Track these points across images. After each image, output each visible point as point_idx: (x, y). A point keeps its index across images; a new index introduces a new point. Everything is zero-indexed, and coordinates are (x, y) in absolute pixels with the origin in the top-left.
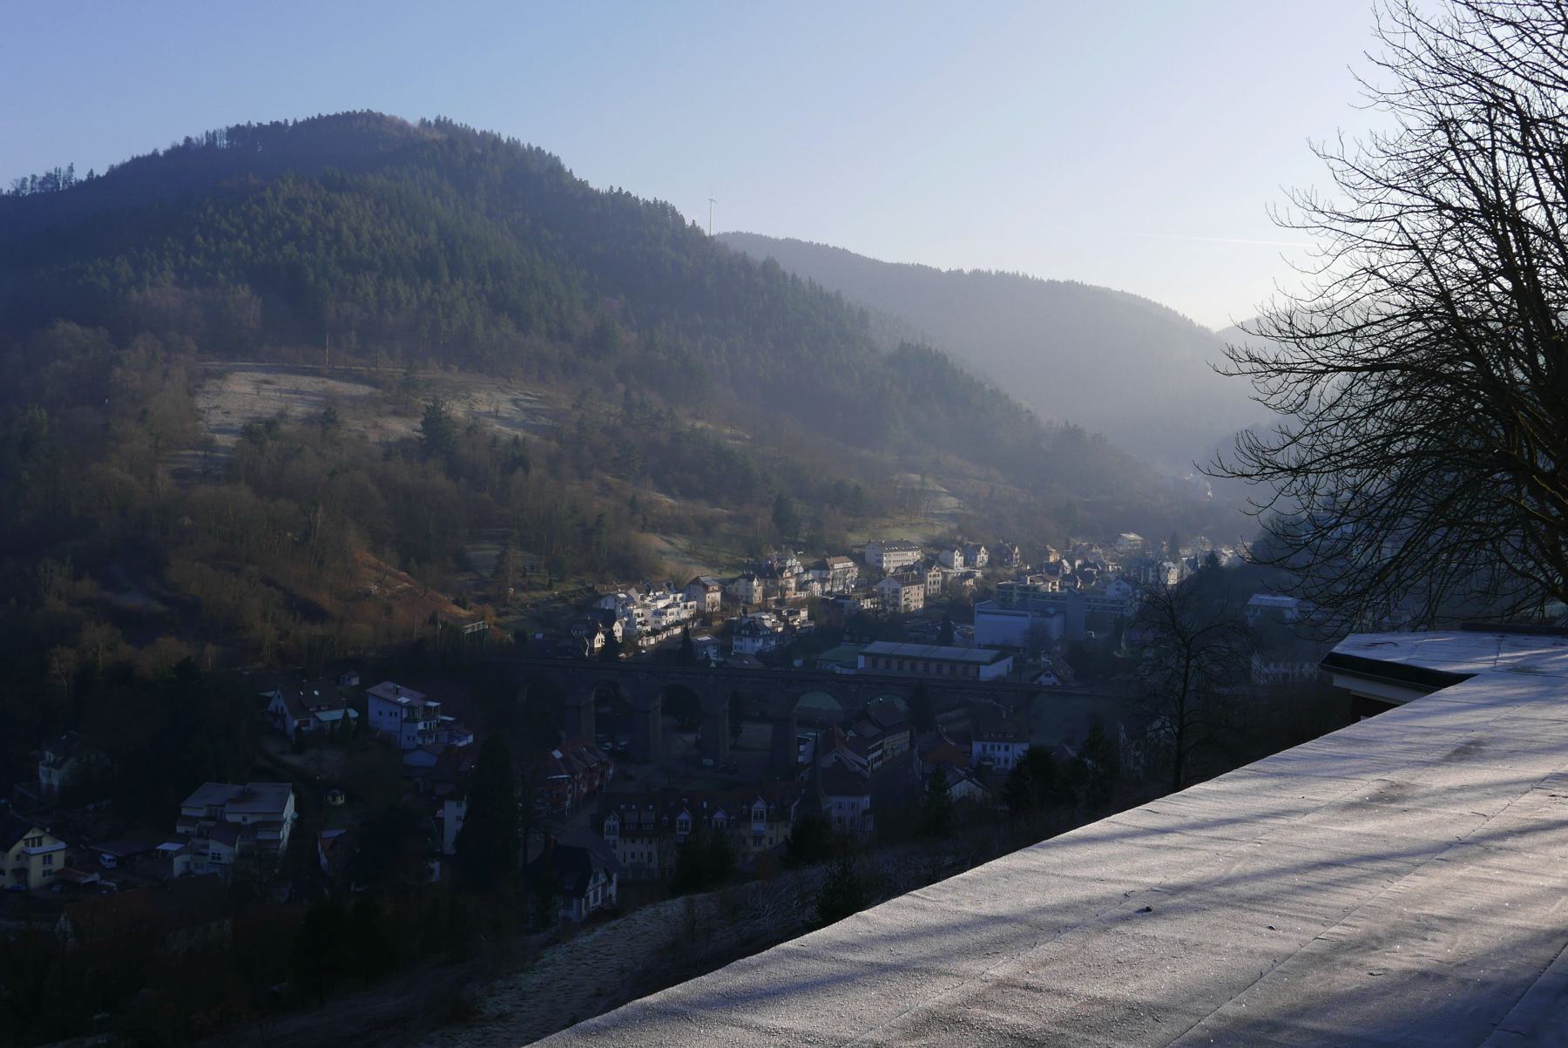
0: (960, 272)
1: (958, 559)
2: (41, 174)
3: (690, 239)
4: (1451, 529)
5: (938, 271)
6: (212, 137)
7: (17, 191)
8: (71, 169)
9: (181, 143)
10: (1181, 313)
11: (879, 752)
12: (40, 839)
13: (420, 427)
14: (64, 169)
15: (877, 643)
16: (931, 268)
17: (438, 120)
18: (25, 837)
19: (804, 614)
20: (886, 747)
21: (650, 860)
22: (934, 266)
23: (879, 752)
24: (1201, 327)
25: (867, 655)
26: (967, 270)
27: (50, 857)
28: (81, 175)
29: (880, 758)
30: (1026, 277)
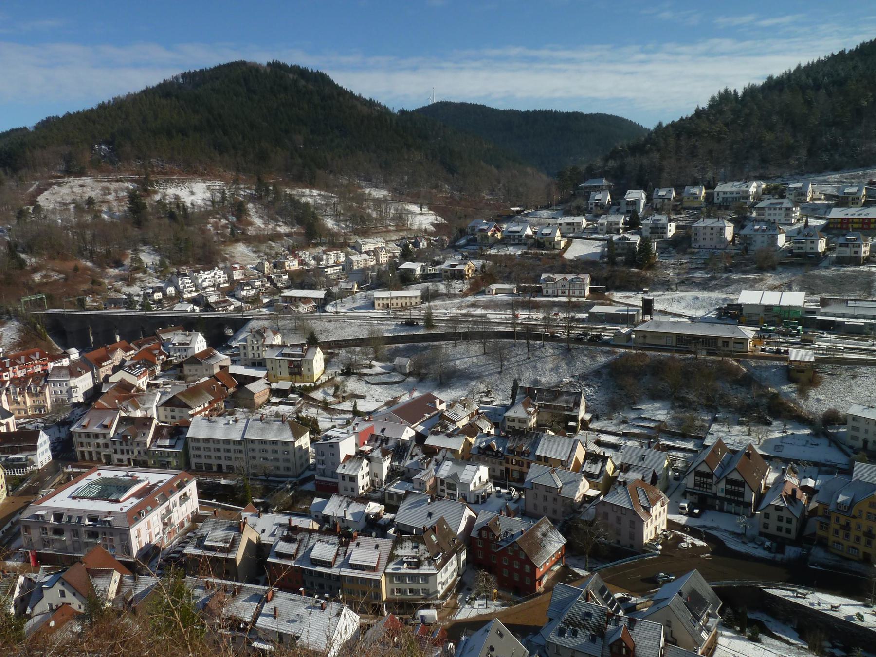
0: (528, 111)
6: (177, 78)
9: (162, 82)
17: (273, 62)
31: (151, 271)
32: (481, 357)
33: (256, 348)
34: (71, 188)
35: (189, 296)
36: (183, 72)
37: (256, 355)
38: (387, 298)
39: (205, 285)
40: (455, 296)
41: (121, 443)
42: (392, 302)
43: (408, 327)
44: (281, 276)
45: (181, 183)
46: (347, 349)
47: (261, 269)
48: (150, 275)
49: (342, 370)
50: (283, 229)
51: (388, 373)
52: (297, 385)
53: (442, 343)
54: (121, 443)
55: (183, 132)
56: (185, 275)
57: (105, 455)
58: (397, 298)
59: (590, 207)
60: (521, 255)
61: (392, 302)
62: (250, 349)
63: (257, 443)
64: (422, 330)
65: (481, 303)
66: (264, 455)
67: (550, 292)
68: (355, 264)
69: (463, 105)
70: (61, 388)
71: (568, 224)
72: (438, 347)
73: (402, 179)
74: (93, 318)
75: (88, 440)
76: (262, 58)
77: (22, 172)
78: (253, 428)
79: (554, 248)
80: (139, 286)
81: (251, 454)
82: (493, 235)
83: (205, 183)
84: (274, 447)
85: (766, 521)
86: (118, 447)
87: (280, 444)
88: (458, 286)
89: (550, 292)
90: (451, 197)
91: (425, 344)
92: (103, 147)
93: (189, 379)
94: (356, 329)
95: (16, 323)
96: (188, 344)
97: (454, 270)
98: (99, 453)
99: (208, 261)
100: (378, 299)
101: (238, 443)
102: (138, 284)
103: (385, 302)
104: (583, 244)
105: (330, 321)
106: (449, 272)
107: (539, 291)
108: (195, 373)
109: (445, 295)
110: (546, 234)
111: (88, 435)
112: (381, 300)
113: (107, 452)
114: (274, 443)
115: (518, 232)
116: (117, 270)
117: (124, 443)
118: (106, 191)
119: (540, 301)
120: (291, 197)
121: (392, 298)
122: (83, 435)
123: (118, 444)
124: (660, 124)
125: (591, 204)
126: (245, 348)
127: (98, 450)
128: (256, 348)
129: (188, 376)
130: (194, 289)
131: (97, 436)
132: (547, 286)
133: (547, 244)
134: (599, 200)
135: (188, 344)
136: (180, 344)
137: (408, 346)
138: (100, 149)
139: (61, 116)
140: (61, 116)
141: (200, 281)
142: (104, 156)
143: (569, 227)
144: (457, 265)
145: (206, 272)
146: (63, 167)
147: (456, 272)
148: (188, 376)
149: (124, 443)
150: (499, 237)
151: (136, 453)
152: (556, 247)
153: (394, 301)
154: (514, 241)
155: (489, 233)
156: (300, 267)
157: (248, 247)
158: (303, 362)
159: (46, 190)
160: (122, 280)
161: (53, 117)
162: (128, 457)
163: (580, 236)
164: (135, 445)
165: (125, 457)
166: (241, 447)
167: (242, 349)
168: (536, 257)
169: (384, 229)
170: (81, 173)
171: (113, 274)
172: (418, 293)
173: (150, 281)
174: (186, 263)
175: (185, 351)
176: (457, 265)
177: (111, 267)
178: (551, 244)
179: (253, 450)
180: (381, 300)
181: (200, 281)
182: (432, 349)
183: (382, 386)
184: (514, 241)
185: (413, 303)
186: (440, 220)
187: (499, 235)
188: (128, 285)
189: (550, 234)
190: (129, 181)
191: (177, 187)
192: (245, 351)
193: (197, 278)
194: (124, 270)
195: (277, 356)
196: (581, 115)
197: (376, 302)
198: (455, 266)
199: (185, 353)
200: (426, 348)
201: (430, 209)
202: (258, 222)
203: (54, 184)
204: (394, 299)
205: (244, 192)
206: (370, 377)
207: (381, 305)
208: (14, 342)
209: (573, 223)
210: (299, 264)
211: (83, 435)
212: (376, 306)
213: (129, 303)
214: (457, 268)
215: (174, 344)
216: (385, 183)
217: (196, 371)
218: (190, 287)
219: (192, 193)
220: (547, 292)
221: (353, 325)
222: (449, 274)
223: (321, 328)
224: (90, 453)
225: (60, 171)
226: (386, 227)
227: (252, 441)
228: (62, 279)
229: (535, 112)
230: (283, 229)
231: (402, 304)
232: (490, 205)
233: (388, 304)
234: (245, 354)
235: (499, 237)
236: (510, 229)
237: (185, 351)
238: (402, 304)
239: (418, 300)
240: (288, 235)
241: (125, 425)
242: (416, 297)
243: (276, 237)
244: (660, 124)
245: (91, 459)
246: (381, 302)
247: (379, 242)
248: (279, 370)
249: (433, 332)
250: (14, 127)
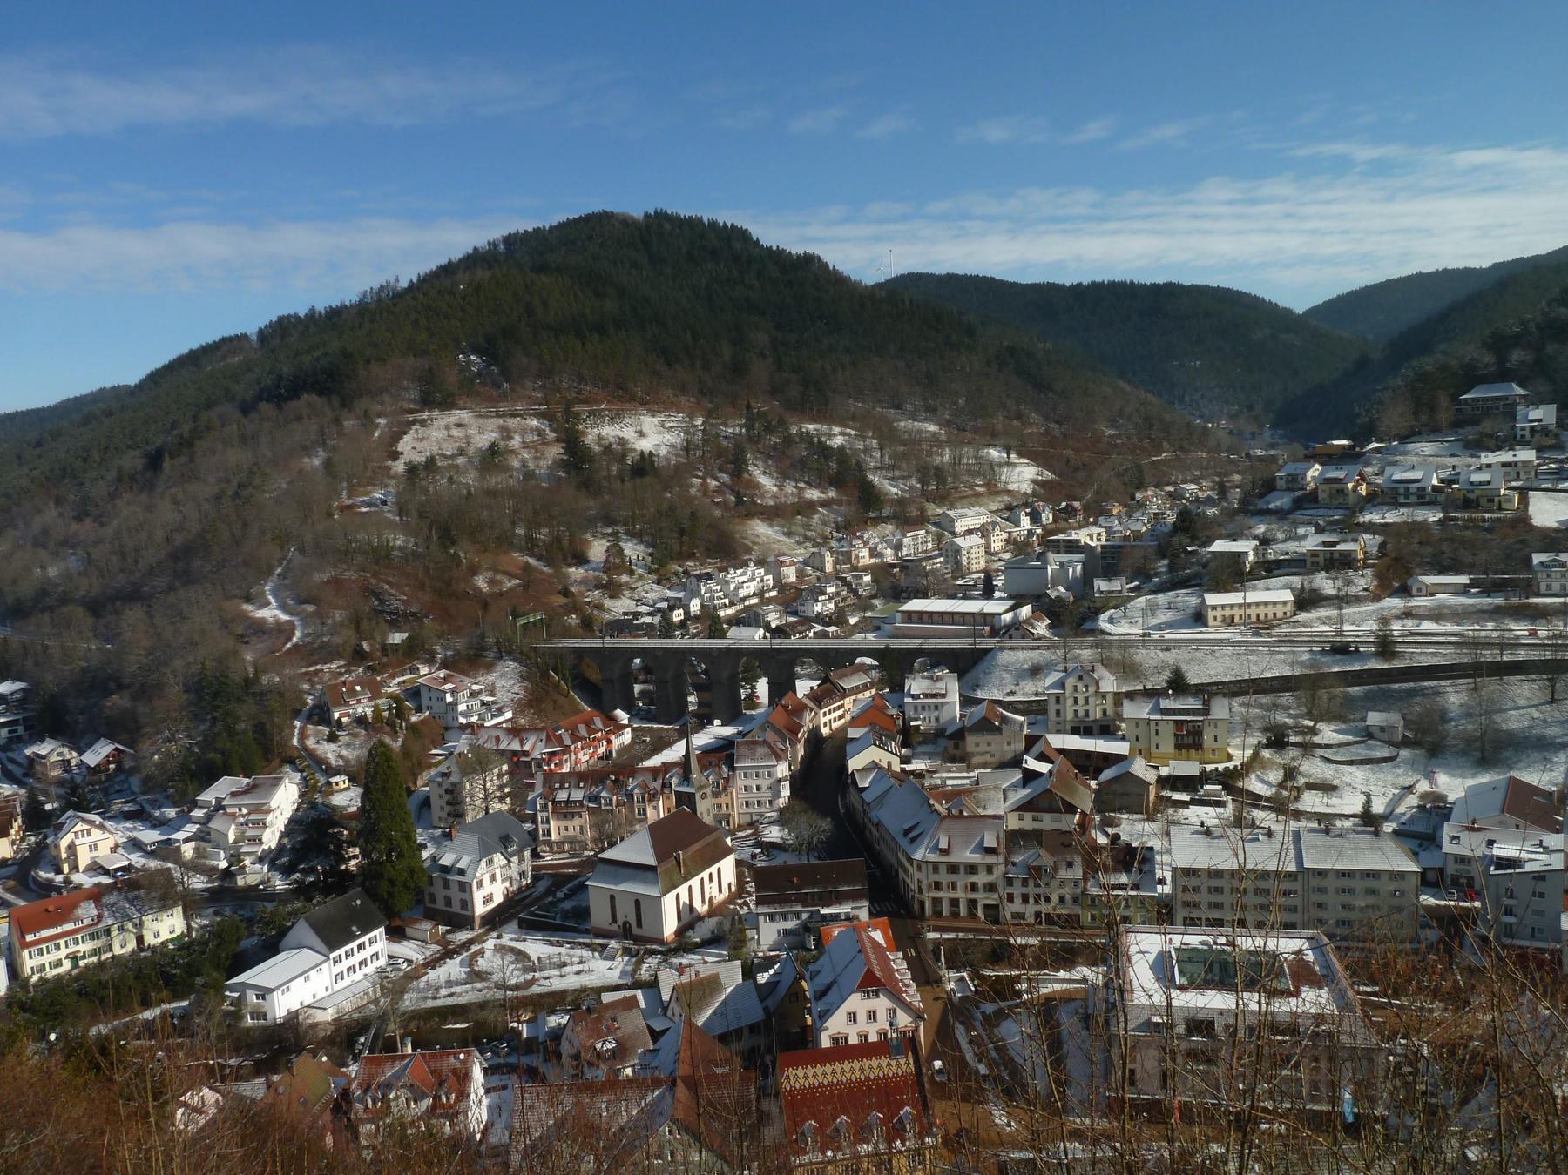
0: (1080, 284)
1: (1025, 522)
2: (376, 286)
3: (838, 280)
4: (309, 899)
5: (1064, 286)
6: (494, 244)
7: (361, 301)
8: (397, 280)
9: (471, 251)
10: (1281, 304)
11: (840, 712)
12: (88, 830)
13: (562, 451)
14: (392, 280)
15: (915, 601)
16: (1270, 302)
17: (656, 212)
18: (74, 830)
19: (867, 578)
20: (847, 708)
21: (582, 832)
22: (1061, 282)
23: (840, 712)
24: (1285, 309)
25: (903, 612)
26: (1085, 283)
27: (96, 846)
28: (404, 284)
29: (841, 717)
30: (1132, 283)
31: (640, 571)
32: (1548, 708)
33: (1081, 701)
34: (447, 427)
35: (729, 611)
36: (505, 234)
37: (1081, 713)
38: (1240, 605)
39: (742, 593)
40: (1357, 600)
41: (1025, 882)
42: (1248, 612)
43: (1338, 657)
44: (861, 577)
45: (616, 417)
46: (1245, 699)
47: (817, 564)
48: (641, 577)
49: (1268, 739)
50: (814, 494)
51: (1363, 742)
52: (1209, 768)
53: (1442, 683)
54: (1025, 882)
55: (599, 329)
56: (709, 577)
57: (986, 907)
58: (1257, 604)
59: (1520, 433)
60: (1440, 522)
61: (1248, 612)
62: (1070, 702)
63: (1385, 878)
64: (1373, 660)
65: (1421, 612)
66: (1346, 898)
67: (1556, 587)
68: (964, 552)
69: (952, 278)
70: (759, 782)
71: (1504, 465)
72: (1436, 692)
73: (955, 404)
74: (660, 654)
75: (953, 877)
76: (636, 206)
77: (362, 404)
78: (1314, 846)
79: (1500, 509)
80: (631, 598)
81: (1317, 898)
82: (1355, 489)
83: (653, 416)
84: (1370, 883)
85: (746, 1032)
86: (1017, 890)
87: (1385, 878)
88: (1363, 581)
89: (1556, 587)
90: (1047, 432)
91: (1406, 686)
92: (473, 358)
93: (976, 760)
94: (1228, 662)
95: (512, 665)
96: (944, 696)
97: (1332, 552)
98: (972, 904)
99: (729, 553)
100: (1214, 608)
101: (1233, 873)
102: (627, 593)
103: (1228, 612)
104: (1555, 499)
105: (1168, 649)
106: (1321, 555)
107: (1530, 588)
108: (988, 749)
109: (1337, 597)
110: (1481, 483)
111: (953, 868)
112: (1219, 609)
113: (992, 899)
114: (1369, 874)
115: (1417, 481)
116: (581, 571)
117: (1031, 883)
118: (507, 434)
119: (1545, 605)
120: (807, 438)
121: (1249, 605)
122: (943, 869)
123: (1018, 884)
124: (313, 310)
125: (1523, 429)
126: (1058, 701)
127: (973, 896)
128: (1081, 701)
129: (973, 755)
130: (727, 601)
131: (972, 869)
132: (1548, 576)
133: (1483, 502)
134: (1540, 420)
135: (944, 696)
136: (926, 696)
137: (1369, 691)
138: (469, 363)
139: (302, 315)
140: (302, 315)
141: (732, 586)
142: (479, 374)
143: (1508, 469)
144: (1337, 543)
145: (738, 572)
146: (414, 394)
147: (1336, 556)
148: (973, 755)
149: (1031, 883)
150: (1364, 493)
151: (1055, 898)
152: (1504, 506)
153: (1253, 611)
154: (1407, 497)
155: (1350, 486)
156: (873, 560)
157: (771, 526)
158: (1206, 724)
159: (405, 433)
160: (597, 587)
161: (289, 316)
162: (1037, 908)
163: (1536, 484)
164: (1054, 883)
165: (1030, 910)
166: (1298, 885)
167: (1052, 701)
168: (1471, 524)
169: (970, 492)
170: (448, 404)
171: (579, 577)
172: (1288, 596)
173: (647, 587)
174: (691, 556)
175: (936, 708)
176: (1337, 543)
177: (570, 566)
178: (1491, 501)
179: (1322, 890)
180: (1219, 609)
181: (732, 586)
182: (1424, 695)
183: (1362, 767)
184: (1407, 497)
185: (1280, 615)
186: (1048, 475)
187: (1363, 490)
188: (612, 597)
189: (1489, 483)
190: (531, 415)
191: (612, 424)
192: (1058, 707)
193: (727, 582)
194: (594, 570)
195: (1149, 714)
196: (1180, 287)
197: (1211, 614)
198: (1334, 544)
199: (936, 714)
200: (1411, 693)
201: (1021, 455)
202: (767, 482)
203: (414, 422)
204: (1270, 606)
205: (734, 429)
206: (1329, 750)
207: (1219, 619)
208: (520, 700)
209: (1516, 464)
210: (872, 556)
211: (943, 869)
212: (1211, 622)
213: (622, 626)
214: (1339, 547)
215: (913, 696)
216: (931, 412)
217: (989, 744)
218: (720, 598)
219: (641, 434)
220: (1549, 587)
221: (1217, 654)
222: (1321, 560)
223: (1153, 663)
224: (954, 903)
225: (411, 401)
226: (971, 487)
227: (1321, 873)
228: (519, 585)
229: (1095, 286)
230: (814, 494)
231: (1258, 616)
232: (1116, 446)
233: (1233, 618)
234: (1058, 712)
235: (1364, 493)
236: (1328, 476)
237: (936, 708)
238: (1258, 616)
239: (1289, 608)
240: (825, 504)
241: (1025, 847)
242: (1285, 603)
243: (808, 508)
244: (313, 310)
245: (955, 915)
246: (1219, 613)
247: (979, 514)
248: (1154, 739)
249: (1398, 664)
250: (226, 335)
